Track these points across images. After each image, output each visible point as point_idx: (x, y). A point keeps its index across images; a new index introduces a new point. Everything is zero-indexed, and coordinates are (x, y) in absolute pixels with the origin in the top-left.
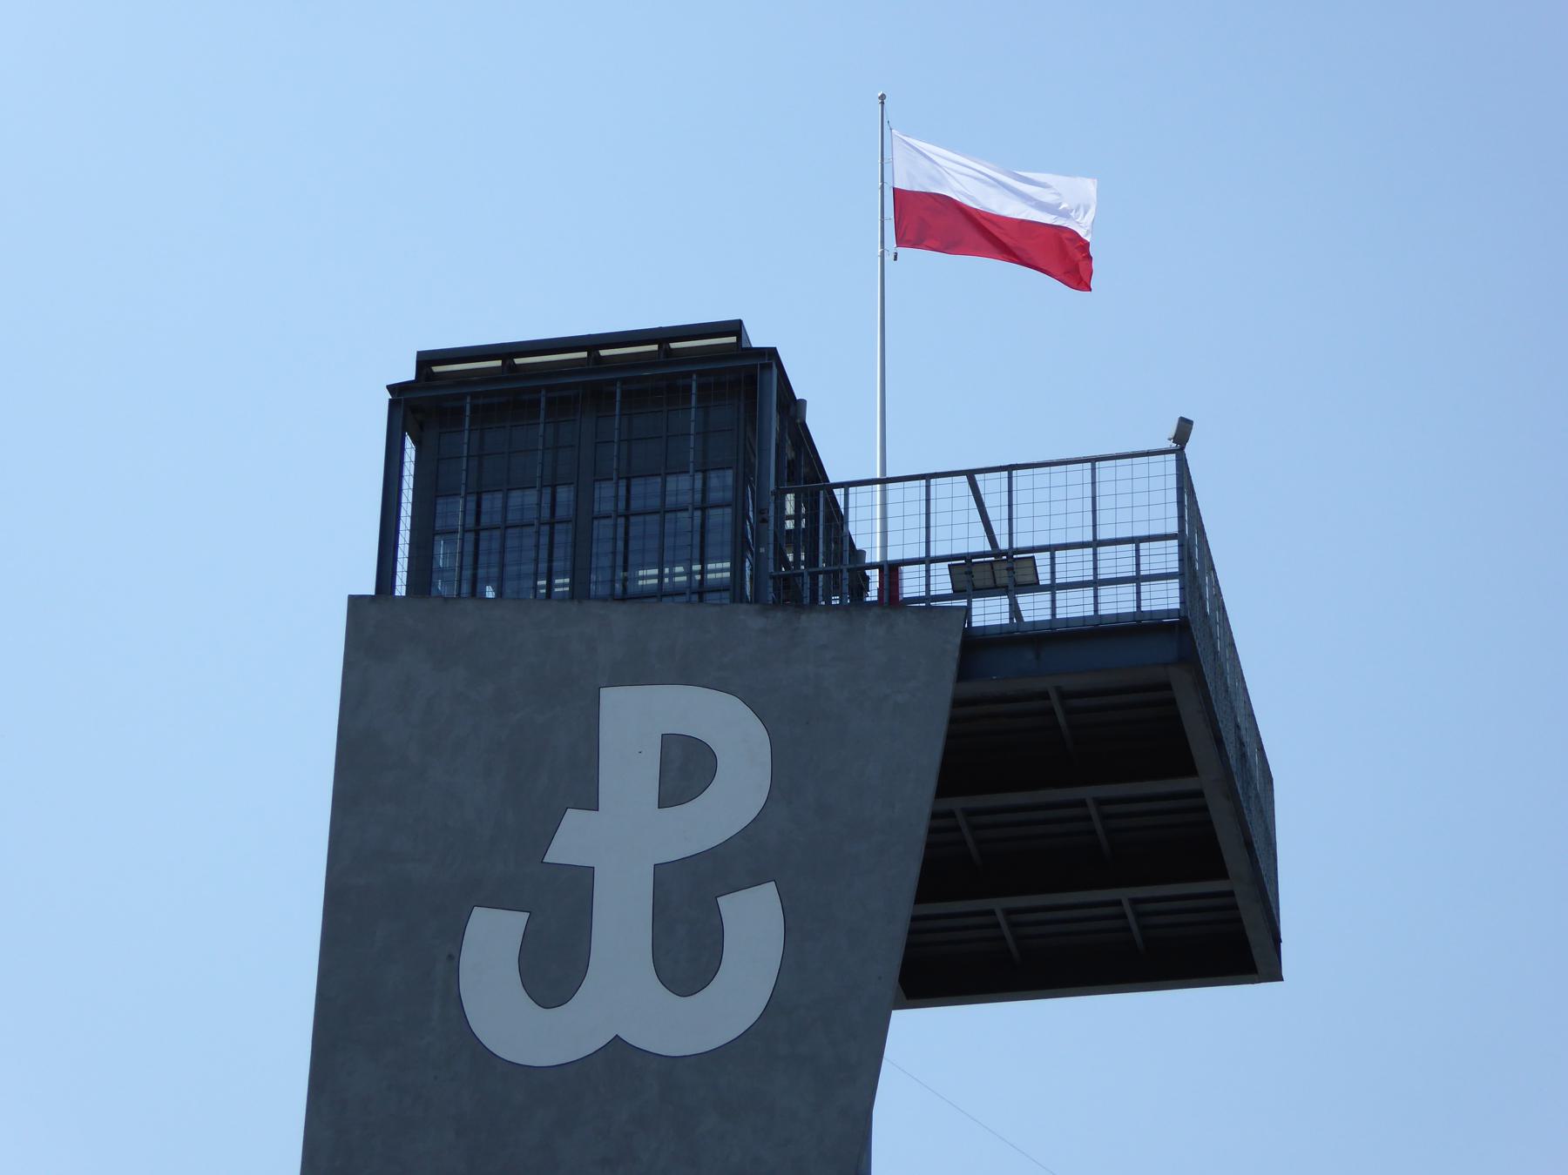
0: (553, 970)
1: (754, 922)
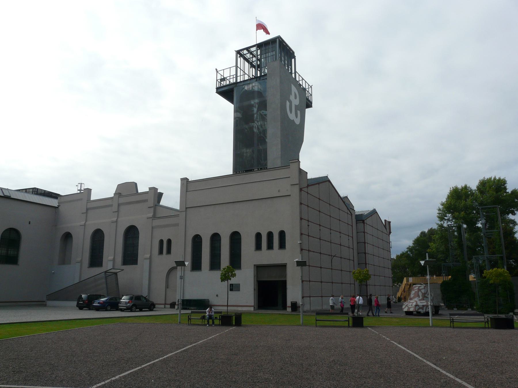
0: (291, 112)
1: (299, 112)
